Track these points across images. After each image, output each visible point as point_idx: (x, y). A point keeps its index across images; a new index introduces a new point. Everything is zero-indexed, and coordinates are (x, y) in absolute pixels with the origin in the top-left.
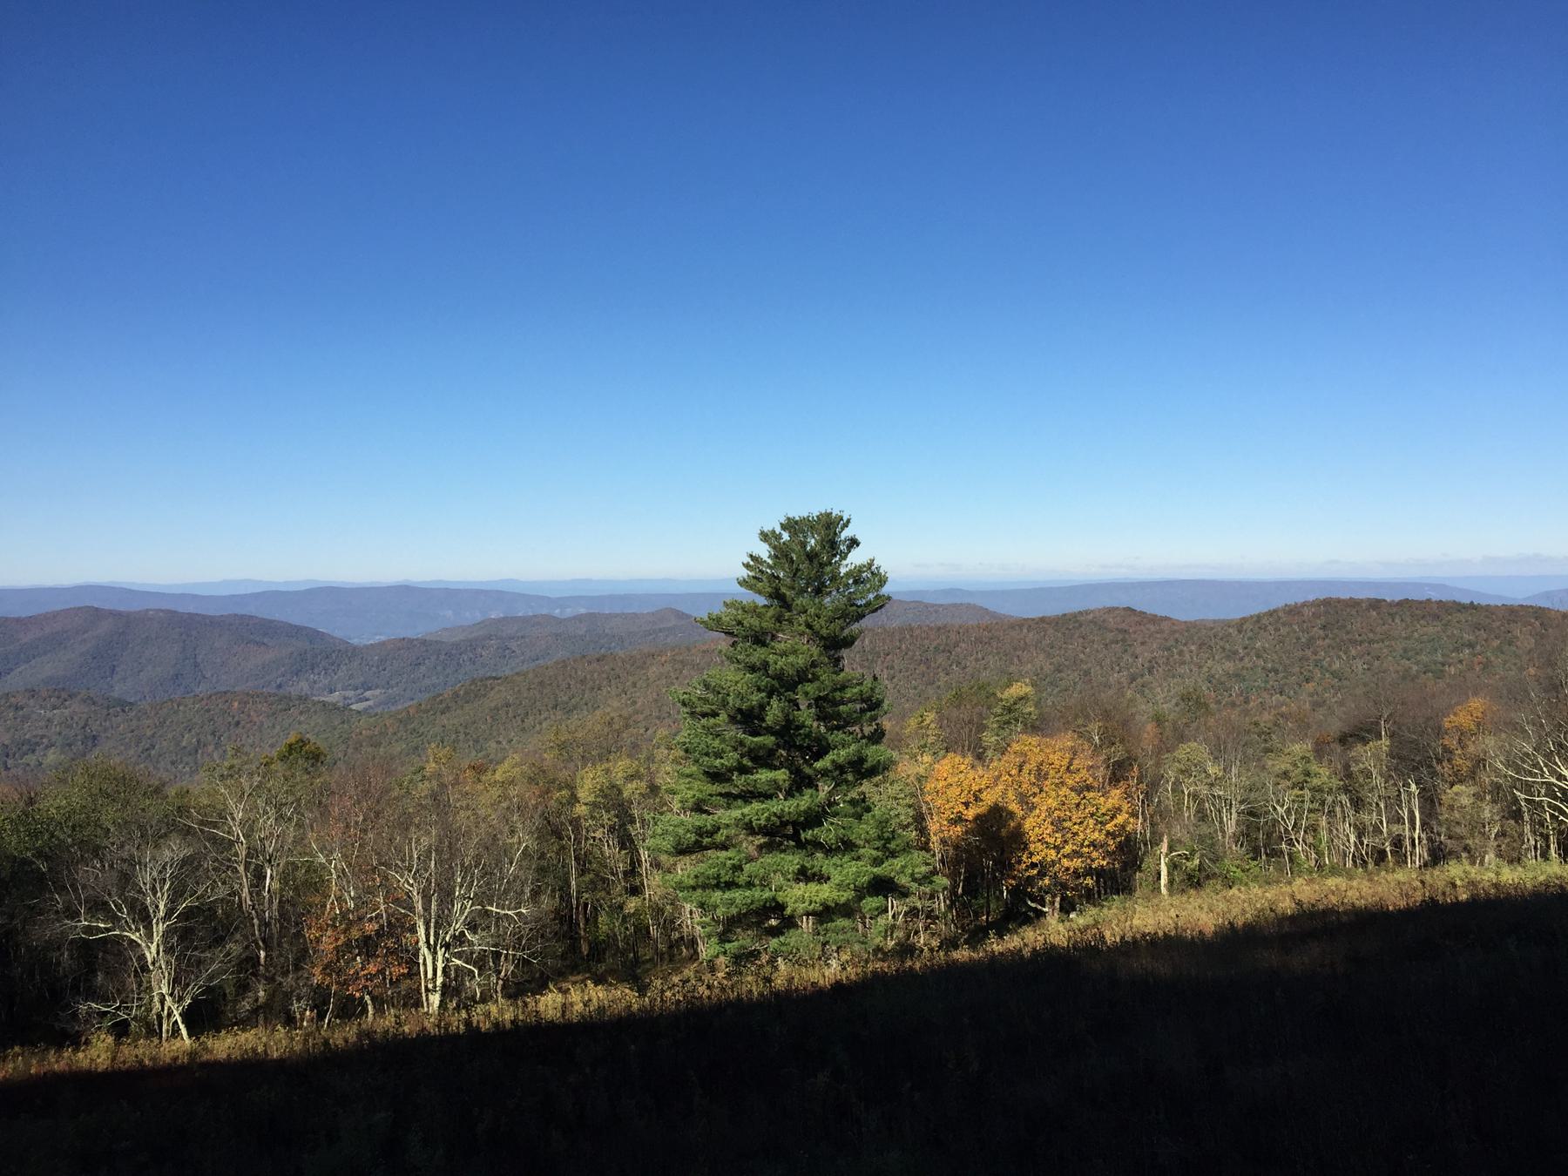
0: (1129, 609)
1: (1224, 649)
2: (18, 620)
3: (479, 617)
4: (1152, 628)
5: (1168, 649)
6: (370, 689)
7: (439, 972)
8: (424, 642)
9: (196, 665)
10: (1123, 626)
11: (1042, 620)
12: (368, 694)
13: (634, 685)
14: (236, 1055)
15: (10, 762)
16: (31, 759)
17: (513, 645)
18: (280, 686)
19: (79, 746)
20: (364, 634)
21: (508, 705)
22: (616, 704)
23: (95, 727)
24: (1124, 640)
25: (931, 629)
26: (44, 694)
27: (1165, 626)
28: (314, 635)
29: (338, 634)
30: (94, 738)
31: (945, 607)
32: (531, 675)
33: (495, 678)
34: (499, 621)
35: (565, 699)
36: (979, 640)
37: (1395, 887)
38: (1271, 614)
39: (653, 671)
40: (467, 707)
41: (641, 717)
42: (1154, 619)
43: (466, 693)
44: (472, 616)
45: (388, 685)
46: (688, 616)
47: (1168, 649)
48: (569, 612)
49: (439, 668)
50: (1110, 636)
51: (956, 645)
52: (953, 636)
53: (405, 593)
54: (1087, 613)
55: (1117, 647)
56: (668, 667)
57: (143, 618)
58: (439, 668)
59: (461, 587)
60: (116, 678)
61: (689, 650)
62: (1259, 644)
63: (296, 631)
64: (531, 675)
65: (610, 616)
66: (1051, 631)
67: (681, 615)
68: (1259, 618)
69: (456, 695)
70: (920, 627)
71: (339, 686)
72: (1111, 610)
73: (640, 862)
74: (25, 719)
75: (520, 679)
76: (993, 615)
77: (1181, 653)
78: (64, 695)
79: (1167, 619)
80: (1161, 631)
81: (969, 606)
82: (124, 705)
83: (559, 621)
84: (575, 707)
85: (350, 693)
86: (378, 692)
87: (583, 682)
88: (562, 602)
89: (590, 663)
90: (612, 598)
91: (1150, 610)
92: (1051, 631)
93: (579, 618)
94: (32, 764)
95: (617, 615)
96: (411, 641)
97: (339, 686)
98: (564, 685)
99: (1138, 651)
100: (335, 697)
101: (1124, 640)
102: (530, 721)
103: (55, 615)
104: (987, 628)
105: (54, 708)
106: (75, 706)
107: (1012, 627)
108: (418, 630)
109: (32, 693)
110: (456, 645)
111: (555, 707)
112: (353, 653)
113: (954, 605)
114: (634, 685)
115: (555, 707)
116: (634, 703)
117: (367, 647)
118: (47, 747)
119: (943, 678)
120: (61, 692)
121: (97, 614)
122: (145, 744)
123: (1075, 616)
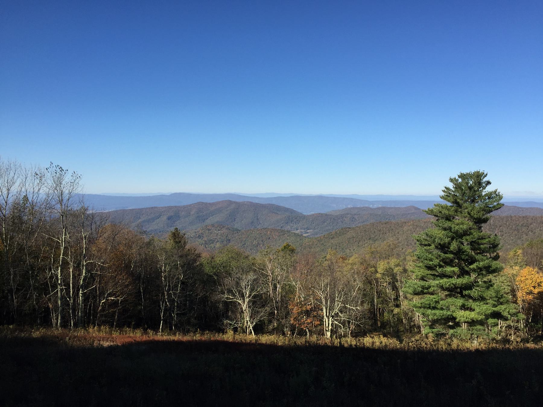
2: (210, 204)
3: (344, 207)
8: (326, 215)
9: (258, 219)
12: (308, 231)
14: (269, 342)
15: (207, 246)
16: (212, 245)
17: (356, 217)
19: (225, 242)
22: (391, 239)
23: (230, 237)
25: (520, 217)
28: (292, 211)
29: (299, 211)
32: (362, 227)
35: (373, 236)
39: (405, 228)
40: (340, 237)
41: (400, 244)
43: (340, 232)
45: (314, 229)
46: (419, 209)
48: (375, 206)
52: (530, 220)
53: (321, 198)
56: (411, 227)
63: (287, 210)
64: (362, 227)
69: (336, 233)
71: (299, 228)
74: (211, 233)
78: (221, 227)
82: (238, 231)
84: (377, 240)
85: (303, 231)
87: (380, 231)
88: (372, 203)
90: (527, 203)
93: (379, 208)
94: (213, 247)
95: (392, 208)
96: (322, 214)
97: (299, 228)
98: (373, 232)
100: (297, 232)
102: (361, 243)
103: (218, 203)
106: (224, 230)
109: (213, 225)
111: (370, 239)
112: (304, 217)
113: (531, 208)
115: (370, 239)
120: (221, 226)
121: (230, 202)
122: (243, 243)
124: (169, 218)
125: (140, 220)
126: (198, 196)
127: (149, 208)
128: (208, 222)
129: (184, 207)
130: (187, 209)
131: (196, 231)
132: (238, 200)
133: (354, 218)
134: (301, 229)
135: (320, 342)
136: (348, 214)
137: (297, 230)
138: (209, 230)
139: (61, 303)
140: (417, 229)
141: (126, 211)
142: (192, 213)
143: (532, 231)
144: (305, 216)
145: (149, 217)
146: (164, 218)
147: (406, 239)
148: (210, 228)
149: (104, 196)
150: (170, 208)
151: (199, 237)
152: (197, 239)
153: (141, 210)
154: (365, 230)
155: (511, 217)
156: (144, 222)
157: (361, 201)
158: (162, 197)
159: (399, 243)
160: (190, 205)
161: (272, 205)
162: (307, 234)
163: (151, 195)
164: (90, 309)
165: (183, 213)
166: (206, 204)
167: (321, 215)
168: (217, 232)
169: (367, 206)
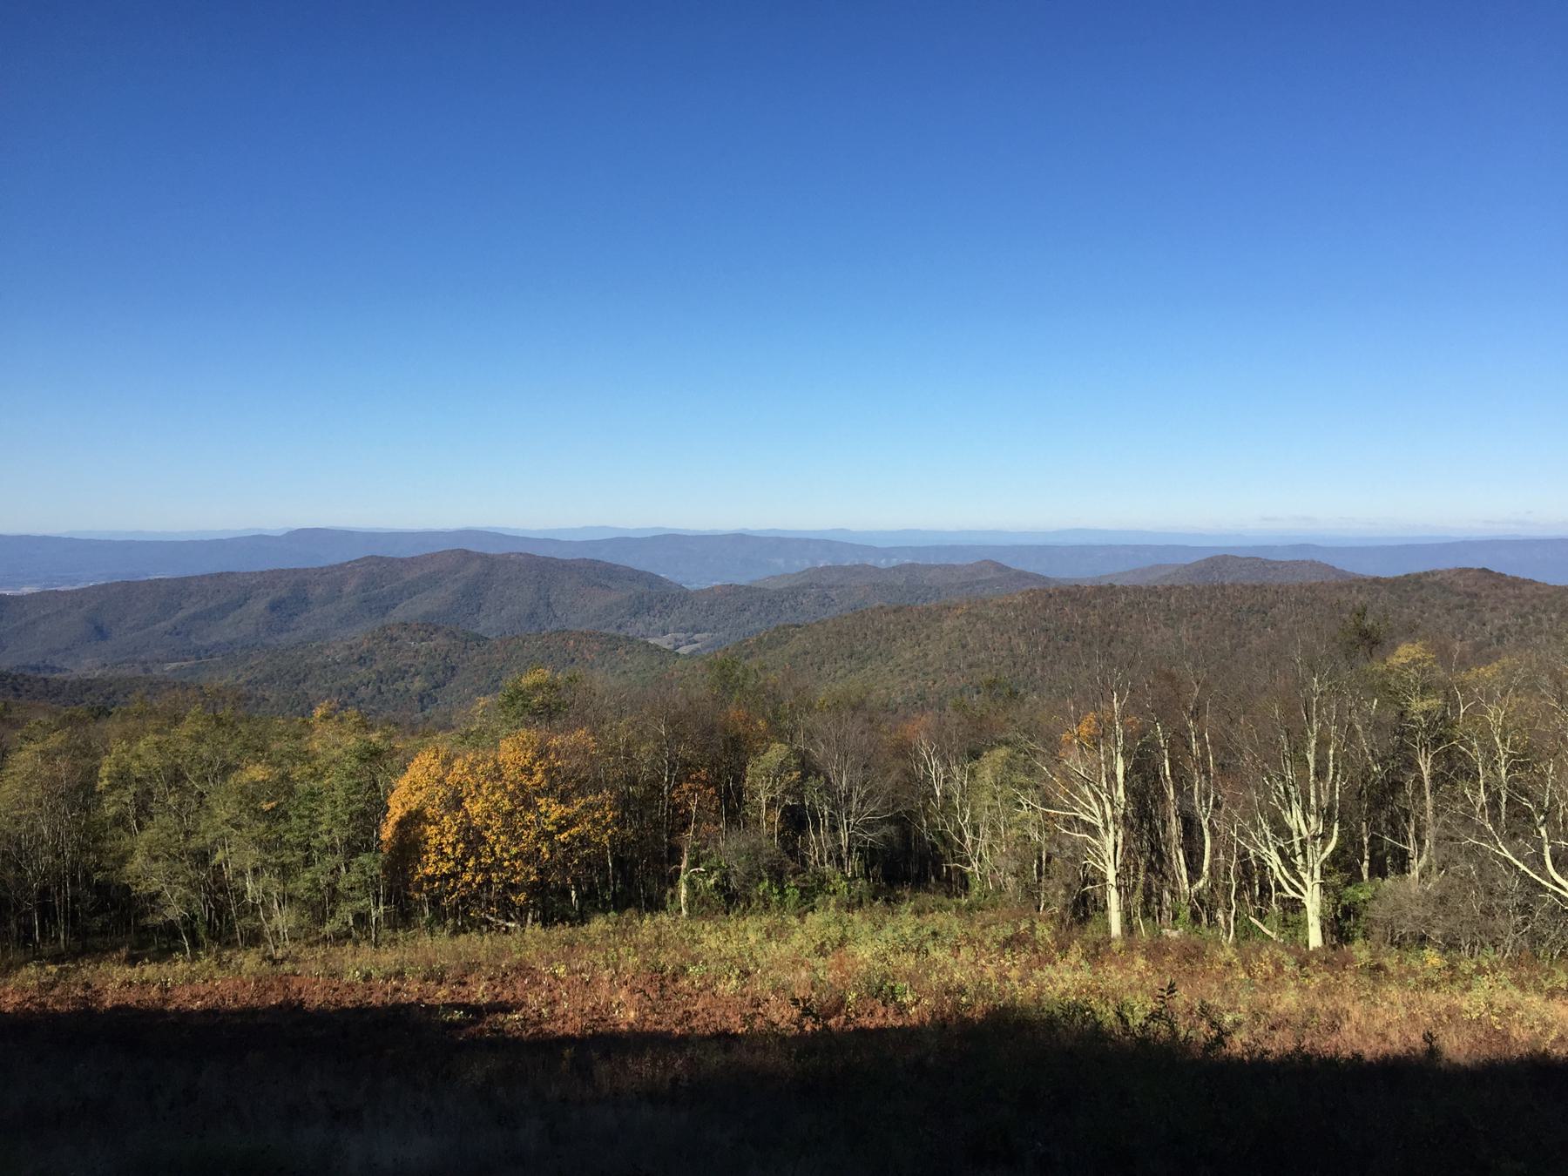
0: (1484, 570)
2: (402, 560)
3: (808, 564)
4: (1511, 592)
7: (1313, 793)
8: (748, 589)
9: (549, 605)
10: (1475, 589)
11: (1376, 580)
12: (697, 637)
13: (928, 637)
15: (384, 688)
16: (401, 685)
17: (833, 594)
18: (619, 627)
19: (440, 676)
20: (696, 579)
22: (908, 655)
24: (1471, 605)
25: (1246, 588)
26: (414, 627)
27: (1527, 590)
28: (652, 580)
29: (678, 579)
30: (453, 668)
31: (1285, 564)
39: (947, 624)
40: (770, 653)
41: (930, 670)
42: (1516, 583)
43: (770, 639)
44: (800, 564)
46: (1008, 569)
48: (894, 562)
50: (1455, 600)
53: (740, 540)
54: (1433, 573)
55: (1462, 613)
57: (505, 560)
60: (482, 614)
61: (985, 603)
63: (636, 576)
64: (830, 624)
65: (930, 568)
66: (1384, 593)
67: (1000, 568)
69: (760, 640)
72: (1463, 572)
73: (163, 955)
74: (398, 649)
77: (1538, 621)
79: (1531, 582)
81: (1312, 564)
82: (480, 639)
85: (681, 636)
86: (705, 635)
87: (879, 632)
88: (887, 552)
90: (938, 549)
91: (1510, 572)
92: (1384, 593)
93: (899, 569)
94: (402, 689)
98: (860, 635)
99: (1488, 616)
100: (664, 642)
101: (1471, 605)
103: (433, 556)
104: (1311, 589)
105: (423, 640)
106: (440, 640)
107: (1340, 588)
109: (405, 626)
111: (851, 656)
113: (1296, 563)
114: (928, 637)
115: (851, 656)
117: (697, 592)
118: (414, 675)
119: (1255, 641)
120: (429, 626)
121: (466, 556)
122: (494, 676)
124: (274, 607)
125: (180, 614)
126: (372, 537)
127: (211, 577)
128: (397, 615)
129: (322, 571)
130: (333, 577)
131: (352, 643)
132: (492, 551)
133: (826, 596)
134: (677, 631)
135: (373, 1000)
136: (811, 586)
137: (664, 633)
138: (392, 639)
140: (979, 626)
141: (137, 584)
142: (347, 589)
143: (1274, 626)
145: (212, 604)
146: (259, 606)
147: (947, 654)
148: (395, 632)
149: (71, 540)
150: (278, 574)
151: (361, 661)
152: (355, 668)
153: (184, 581)
155: (1223, 587)
156: (194, 617)
157: (853, 547)
158: (258, 542)
159: (927, 665)
160: (341, 566)
161: (593, 564)
163: (224, 537)
164: (1097, 798)
165: (319, 590)
166: (391, 561)
167: (735, 590)
168: (418, 646)
169: (870, 562)
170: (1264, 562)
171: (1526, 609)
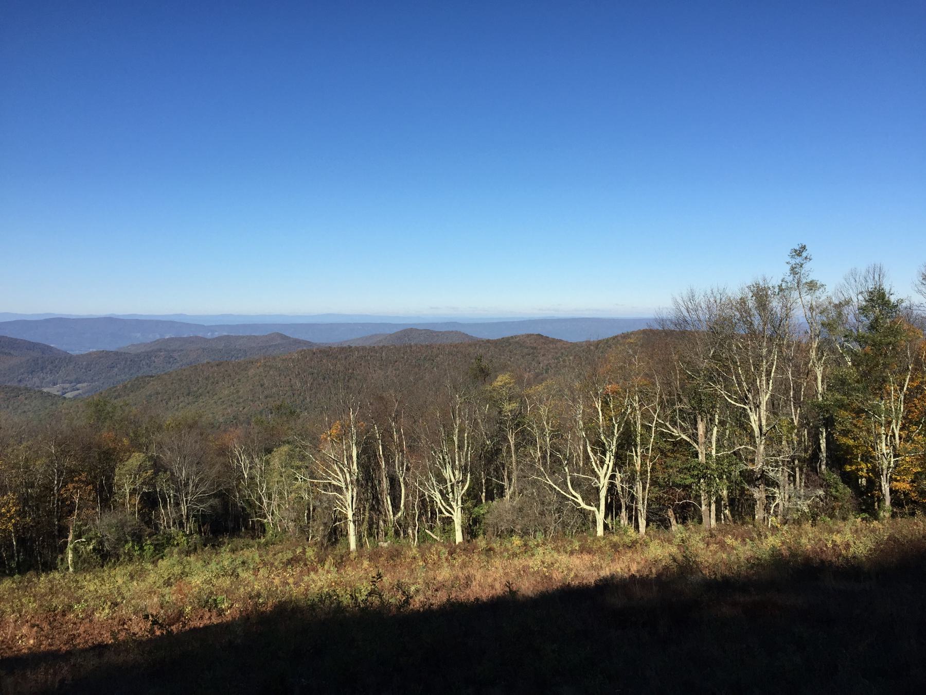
0: (539, 335)
1: (587, 358)
3: (158, 337)
5: (557, 359)
6: (80, 383)
8: (116, 353)
11: (488, 341)
12: (79, 386)
13: (239, 380)
17: (176, 355)
18: (20, 381)
20: (77, 348)
21: (158, 393)
22: (226, 392)
27: (559, 345)
28: (45, 349)
31: (443, 333)
32: (174, 375)
33: (152, 377)
34: (171, 339)
35: (195, 389)
36: (450, 353)
37: (647, 551)
38: (614, 338)
39: (251, 372)
40: (132, 395)
42: (554, 341)
43: (132, 385)
46: (288, 338)
47: (557, 359)
48: (217, 334)
49: (126, 370)
50: (526, 351)
51: (437, 356)
52: (435, 350)
53: (110, 321)
54: (516, 337)
56: (261, 369)
58: (126, 370)
59: (148, 319)
61: (274, 359)
62: (156, 599)
63: (32, 346)
64: (174, 375)
68: (607, 340)
69: (125, 387)
70: (416, 345)
71: (60, 381)
72: (529, 336)
75: (167, 377)
76: (471, 338)
77: (564, 361)
79: (560, 341)
80: (556, 348)
83: (206, 340)
85: (67, 385)
86: (85, 385)
87: (207, 379)
88: (211, 328)
89: (212, 367)
90: (245, 326)
92: (492, 348)
93: (220, 339)
95: (243, 337)
96: (107, 352)
97: (60, 381)
99: (541, 359)
101: (533, 353)
102: (172, 403)
107: (470, 345)
108: (112, 346)
110: (138, 355)
111: (188, 394)
112: (67, 359)
114: (239, 380)
115: (188, 394)
116: (238, 392)
117: (78, 356)
123: (508, 339)
134: (63, 383)
136: (160, 350)
137: (54, 384)
139: (874, 505)
140: (271, 373)
144: (71, 356)
147: (251, 390)
154: (180, 380)
155: (411, 346)
157: (188, 326)
162: (76, 392)
167: (107, 354)
169: (201, 335)
170: (432, 332)
171: (559, 354)
